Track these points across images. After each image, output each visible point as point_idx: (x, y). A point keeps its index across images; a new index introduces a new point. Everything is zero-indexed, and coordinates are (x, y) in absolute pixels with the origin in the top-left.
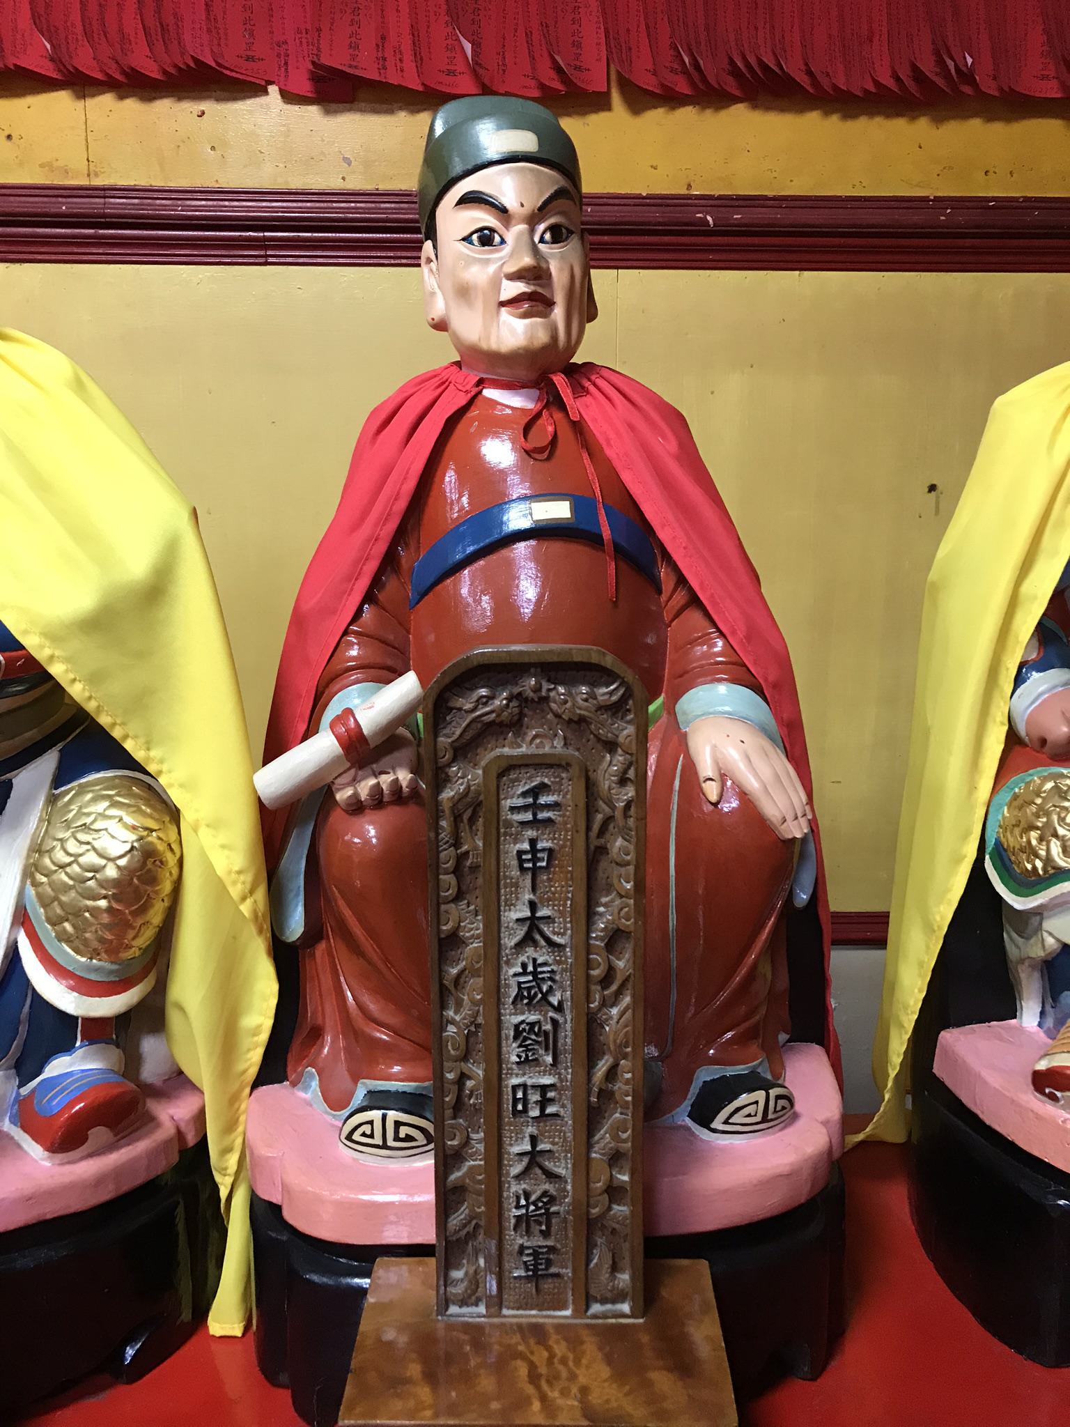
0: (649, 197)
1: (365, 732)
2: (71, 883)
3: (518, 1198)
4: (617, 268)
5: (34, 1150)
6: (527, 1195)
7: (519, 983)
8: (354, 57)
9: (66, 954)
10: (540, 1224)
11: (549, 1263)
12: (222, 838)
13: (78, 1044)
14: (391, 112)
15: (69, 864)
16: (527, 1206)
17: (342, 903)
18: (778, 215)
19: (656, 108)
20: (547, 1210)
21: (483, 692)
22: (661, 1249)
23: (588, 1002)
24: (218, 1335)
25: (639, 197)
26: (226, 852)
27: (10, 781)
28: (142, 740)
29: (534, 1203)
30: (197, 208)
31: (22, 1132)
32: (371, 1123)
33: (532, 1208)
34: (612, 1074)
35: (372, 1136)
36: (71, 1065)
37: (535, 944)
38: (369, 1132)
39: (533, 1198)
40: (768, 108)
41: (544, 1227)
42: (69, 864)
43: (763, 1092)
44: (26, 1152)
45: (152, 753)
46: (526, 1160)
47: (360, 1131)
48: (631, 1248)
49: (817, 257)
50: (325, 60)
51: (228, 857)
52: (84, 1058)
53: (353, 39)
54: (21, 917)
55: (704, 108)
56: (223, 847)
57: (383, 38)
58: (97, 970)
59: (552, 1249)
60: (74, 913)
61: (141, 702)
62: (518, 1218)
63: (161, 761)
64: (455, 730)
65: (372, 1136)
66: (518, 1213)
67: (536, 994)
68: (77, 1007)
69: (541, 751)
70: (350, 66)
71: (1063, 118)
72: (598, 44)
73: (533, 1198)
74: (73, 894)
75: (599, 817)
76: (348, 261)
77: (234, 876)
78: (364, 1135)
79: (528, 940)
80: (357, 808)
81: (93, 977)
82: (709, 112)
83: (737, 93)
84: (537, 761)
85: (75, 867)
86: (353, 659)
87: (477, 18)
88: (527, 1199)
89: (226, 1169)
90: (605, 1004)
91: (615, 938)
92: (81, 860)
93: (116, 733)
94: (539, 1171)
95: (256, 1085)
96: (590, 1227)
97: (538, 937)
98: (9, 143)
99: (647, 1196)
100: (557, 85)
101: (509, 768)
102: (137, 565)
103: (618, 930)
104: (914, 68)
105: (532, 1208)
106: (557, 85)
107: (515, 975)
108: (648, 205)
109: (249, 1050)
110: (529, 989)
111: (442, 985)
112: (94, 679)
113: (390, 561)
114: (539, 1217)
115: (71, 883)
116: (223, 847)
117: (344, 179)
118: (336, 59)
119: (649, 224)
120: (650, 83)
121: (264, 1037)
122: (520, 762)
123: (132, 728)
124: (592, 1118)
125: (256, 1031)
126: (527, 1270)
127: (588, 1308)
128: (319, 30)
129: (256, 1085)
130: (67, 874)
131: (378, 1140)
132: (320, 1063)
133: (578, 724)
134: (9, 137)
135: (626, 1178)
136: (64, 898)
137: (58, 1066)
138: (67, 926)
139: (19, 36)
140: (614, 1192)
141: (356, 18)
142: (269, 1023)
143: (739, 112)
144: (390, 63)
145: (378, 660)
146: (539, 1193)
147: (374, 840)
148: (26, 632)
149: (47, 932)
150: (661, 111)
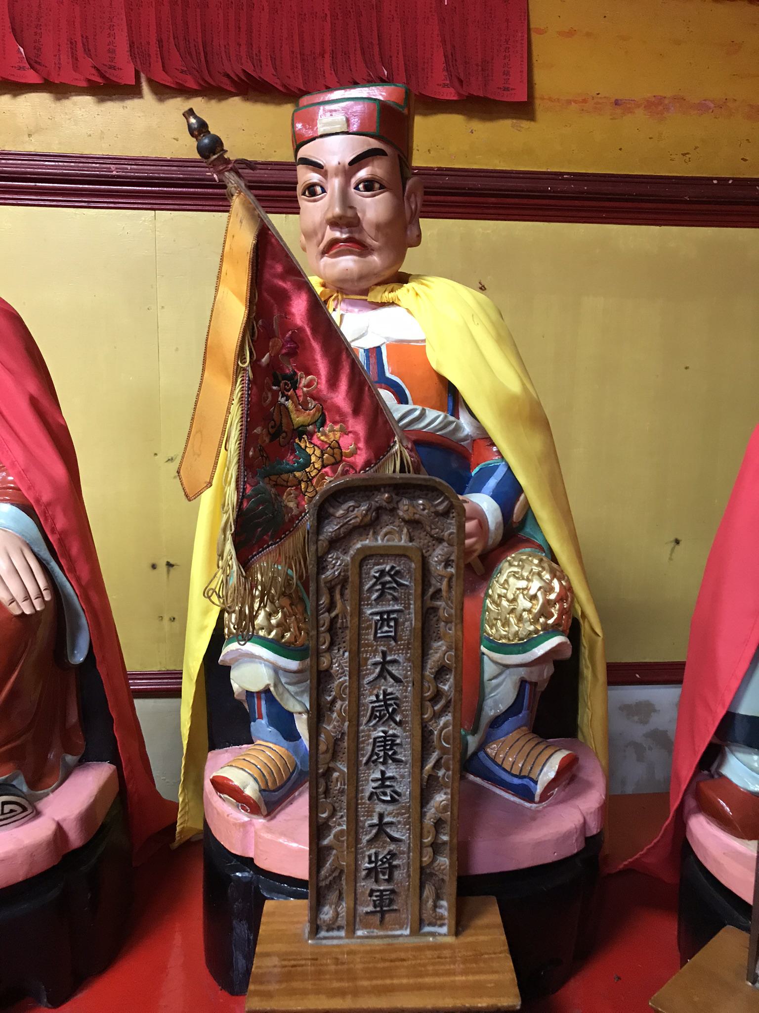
3: (370, 857)
6: (376, 854)
7: (373, 707)
11: (391, 902)
18: (510, 184)
20: (390, 864)
21: (351, 503)
22: (471, 888)
23: (422, 714)
29: (381, 860)
30: (7, 165)
33: (380, 863)
34: (437, 765)
39: (380, 858)
40: (256, 101)
41: (387, 877)
46: (374, 580)
48: (450, 888)
49: (584, 214)
55: (210, 99)
59: (393, 891)
62: (369, 870)
64: (331, 529)
66: (367, 865)
67: (385, 715)
69: (390, 543)
71: (50, 92)
73: (380, 858)
75: (431, 590)
76: (105, 205)
79: (380, 675)
82: (213, 102)
83: (233, 90)
84: (397, 552)
87: (112, 32)
88: (376, 857)
90: (437, 716)
91: (441, 672)
96: (425, 874)
97: (386, 674)
99: (463, 852)
100: (100, 80)
101: (366, 557)
103: (444, 666)
104: (244, 71)
106: (100, 80)
107: (375, 702)
108: (481, 176)
110: (380, 711)
111: (318, 605)
114: (384, 869)
119: (262, 182)
120: (168, 81)
122: (382, 552)
124: (425, 797)
126: (375, 906)
127: (420, 928)
133: (414, 524)
141: (112, 32)
143: (236, 101)
146: (386, 852)
150: (179, 99)
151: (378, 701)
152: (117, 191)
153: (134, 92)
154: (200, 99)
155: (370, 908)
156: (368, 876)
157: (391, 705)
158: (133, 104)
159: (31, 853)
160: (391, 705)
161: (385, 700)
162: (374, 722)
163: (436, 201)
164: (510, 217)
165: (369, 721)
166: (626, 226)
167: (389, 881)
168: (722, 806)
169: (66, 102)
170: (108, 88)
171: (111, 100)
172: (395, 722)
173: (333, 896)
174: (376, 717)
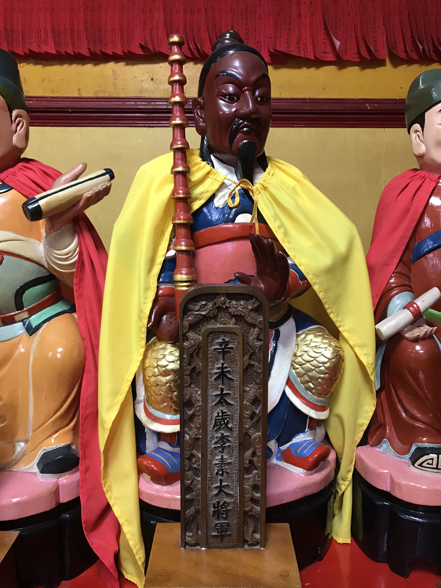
0: (400, 100)
1: (422, 310)
2: (314, 368)
4: (384, 128)
5: (298, 471)
8: (289, 47)
9: (309, 395)
10: (223, 514)
12: (365, 351)
13: (306, 430)
14: (300, 67)
15: (312, 361)
16: (218, 507)
17: (409, 376)
19: (402, 65)
24: (341, 542)
25: (396, 100)
26: (366, 356)
27: (278, 329)
28: (336, 314)
29: (221, 506)
31: (286, 464)
32: (432, 459)
35: (432, 464)
36: (304, 438)
37: (222, 403)
38: (431, 463)
42: (312, 361)
43: (436, 456)
44: (291, 472)
45: (338, 319)
47: (427, 462)
50: (278, 49)
51: (367, 358)
52: (308, 436)
53: (288, 41)
54: (289, 382)
56: (365, 354)
57: (299, 39)
58: (320, 401)
60: (312, 379)
61: (337, 300)
63: (341, 322)
65: (432, 464)
68: (316, 415)
70: (288, 51)
72: (383, 41)
74: (314, 372)
77: (370, 365)
78: (428, 464)
79: (219, 402)
80: (416, 340)
81: (319, 404)
83: (436, 59)
85: (315, 362)
86: (393, 283)
89: (347, 479)
92: (317, 359)
93: (329, 311)
94: (223, 494)
95: (358, 446)
98: (152, 82)
100: (368, 57)
102: (342, 247)
105: (220, 508)
106: (368, 57)
109: (358, 433)
112: (327, 291)
113: (407, 247)
115: (314, 368)
116: (365, 354)
117: (280, 94)
118: (282, 48)
120: (403, 55)
121: (365, 427)
123: (334, 310)
125: (361, 426)
128: (276, 37)
129: (358, 446)
130: (311, 364)
131: (434, 466)
132: (388, 436)
134: (152, 79)
135: (259, 495)
136: (309, 374)
137: (299, 438)
138: (311, 384)
139: (159, 40)
140: (253, 500)
142: (367, 422)
144: (301, 50)
145: (401, 283)
147: (59, 356)
148: (308, 273)
149: (301, 388)
150: (405, 66)
151: (218, 416)
152: (128, 117)
153: (382, 63)
154: (416, 65)
155: (215, 533)
156: (213, 515)
157: (226, 418)
158: (380, 70)
159: (314, 484)
160: (226, 418)
161: (222, 416)
162: (216, 428)
163: (307, 118)
164: (357, 126)
165: (214, 427)
166: (394, 129)
167: (225, 519)
168: (414, 486)
169: (345, 71)
170: (370, 61)
171: (369, 68)
172: (228, 427)
173: (194, 526)
174: (218, 425)
